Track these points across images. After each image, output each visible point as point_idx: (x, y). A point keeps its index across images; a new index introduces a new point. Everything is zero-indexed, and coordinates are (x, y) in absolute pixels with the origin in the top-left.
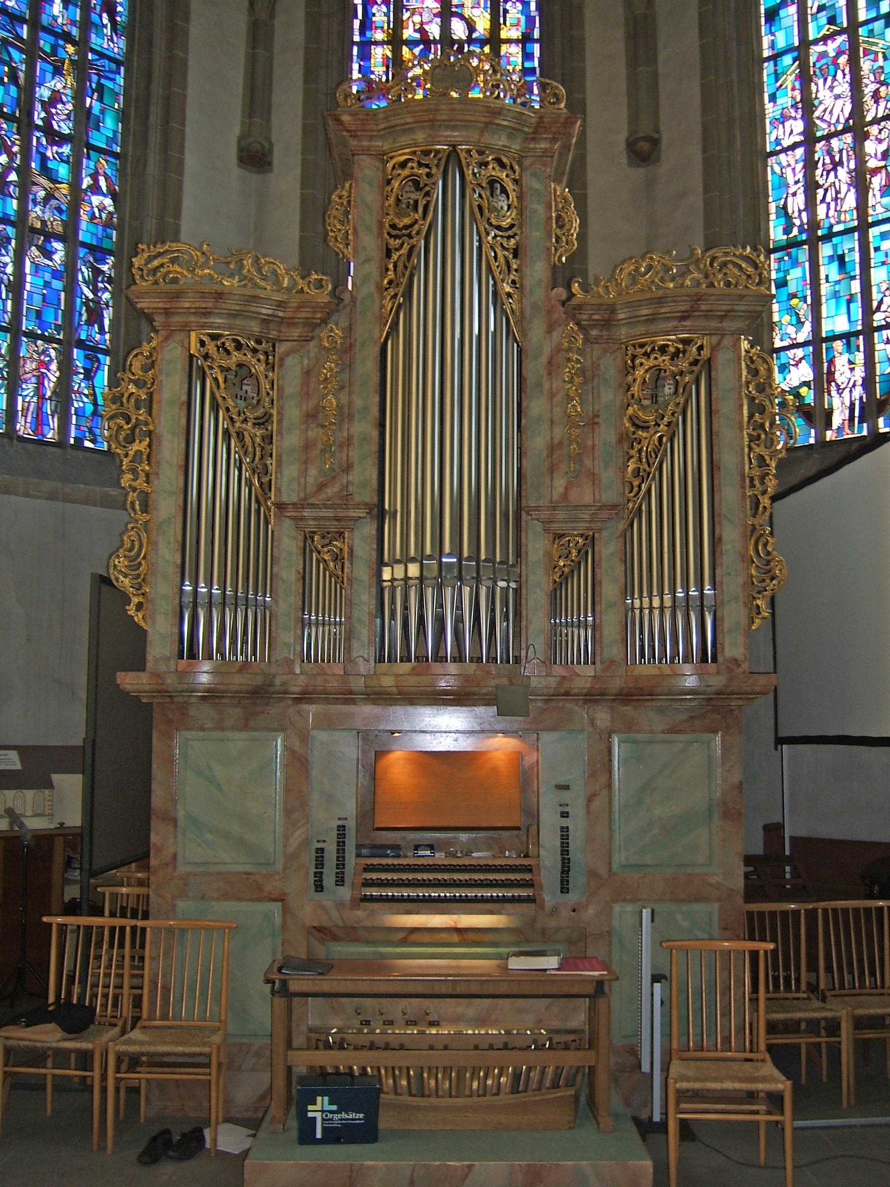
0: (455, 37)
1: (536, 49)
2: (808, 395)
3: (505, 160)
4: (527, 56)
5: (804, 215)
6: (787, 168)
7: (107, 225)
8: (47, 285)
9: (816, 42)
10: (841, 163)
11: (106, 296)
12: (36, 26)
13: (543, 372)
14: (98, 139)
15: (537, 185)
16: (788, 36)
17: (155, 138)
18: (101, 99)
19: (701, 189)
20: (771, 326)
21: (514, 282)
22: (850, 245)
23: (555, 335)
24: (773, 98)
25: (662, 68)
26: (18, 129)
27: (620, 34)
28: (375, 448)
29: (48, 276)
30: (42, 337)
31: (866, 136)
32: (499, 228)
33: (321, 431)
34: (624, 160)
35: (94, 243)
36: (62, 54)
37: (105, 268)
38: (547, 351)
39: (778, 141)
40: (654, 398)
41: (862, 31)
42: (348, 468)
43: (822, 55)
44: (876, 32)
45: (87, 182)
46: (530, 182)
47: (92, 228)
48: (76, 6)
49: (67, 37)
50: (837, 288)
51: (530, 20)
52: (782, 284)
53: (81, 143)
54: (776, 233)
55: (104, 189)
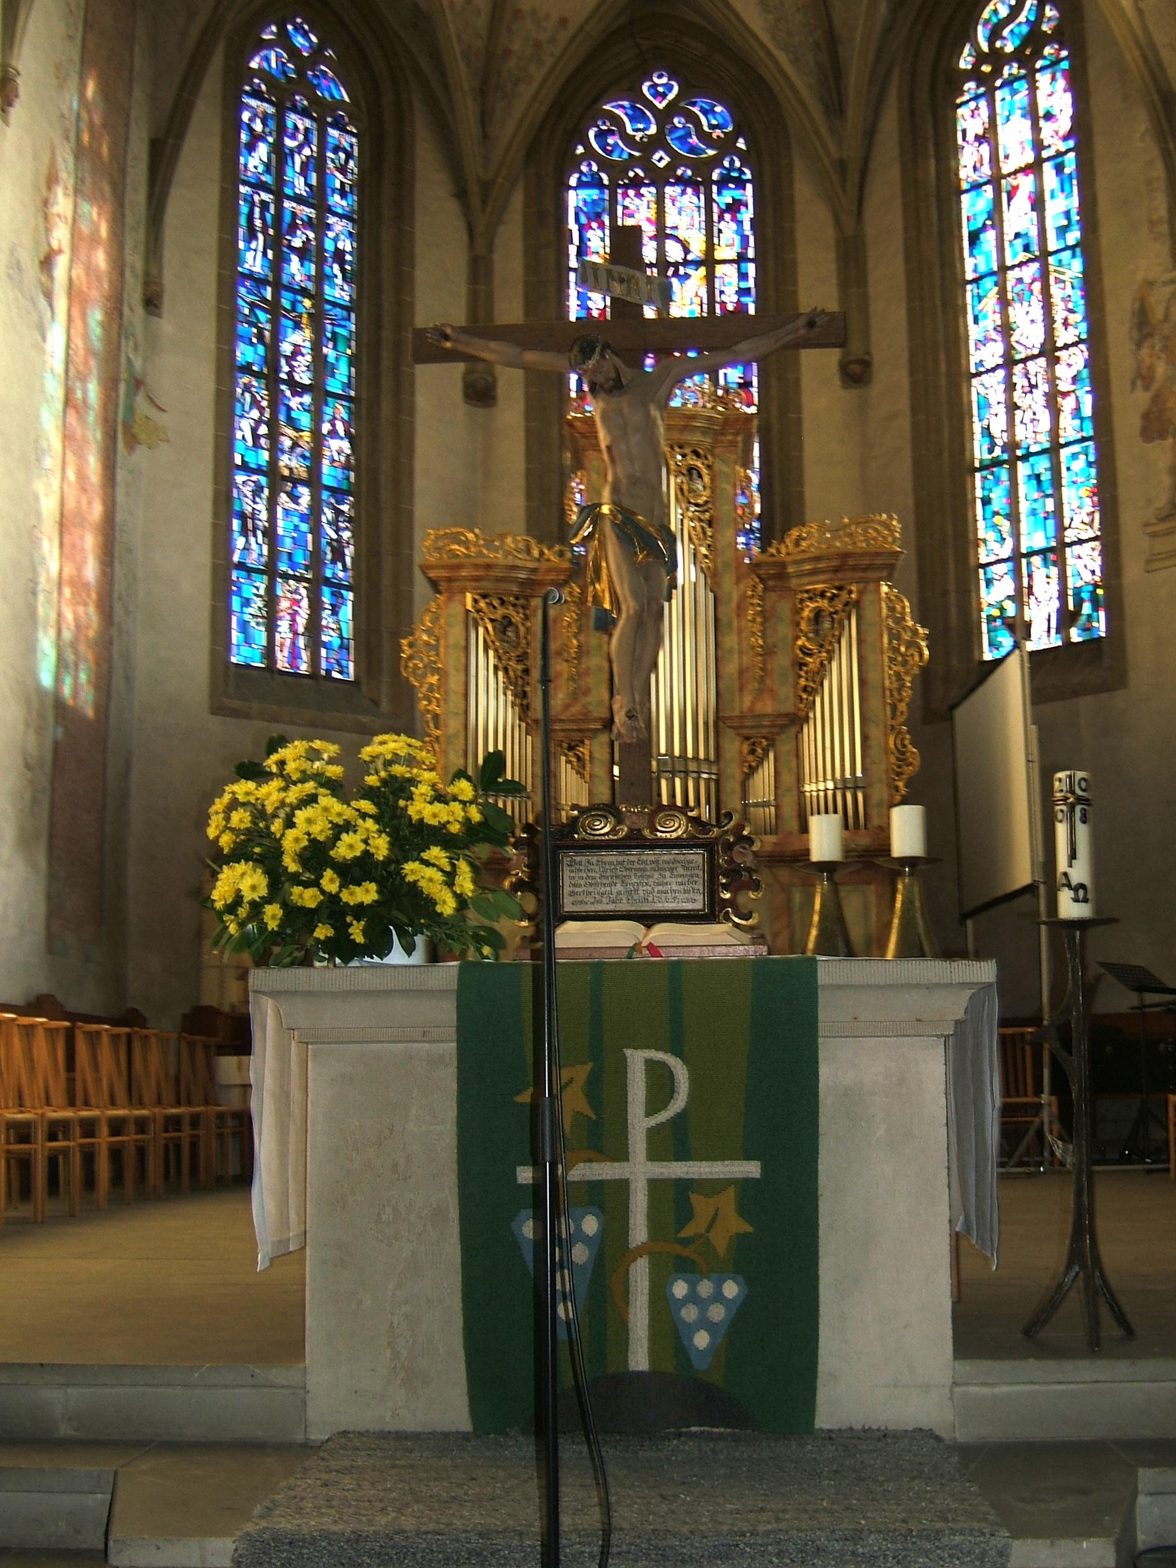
0: (669, 259)
1: (751, 269)
2: (1011, 609)
3: (701, 452)
4: (743, 276)
5: (1005, 435)
6: (988, 389)
7: (347, 467)
8: (296, 528)
9: (1013, 267)
10: (1036, 386)
11: (346, 535)
12: (278, 286)
13: (734, 614)
14: (334, 386)
15: (725, 469)
16: (988, 260)
17: (386, 383)
18: (335, 348)
19: (908, 412)
20: (977, 542)
21: (709, 546)
22: (1042, 464)
23: (742, 586)
24: (976, 321)
25: (872, 291)
26: (267, 385)
27: (832, 255)
28: (606, 676)
29: (296, 520)
30: (295, 578)
31: (1057, 360)
32: (697, 505)
33: (565, 664)
34: (837, 381)
35: (335, 485)
36: (300, 309)
37: (345, 508)
38: (735, 597)
39: (980, 363)
40: (817, 632)
41: (1051, 260)
42: (587, 692)
43: (1020, 281)
44: (1064, 262)
45: (326, 428)
46: (719, 466)
47: (333, 472)
48: (311, 261)
49: (304, 292)
50: (1035, 506)
51: (744, 239)
52: (986, 501)
53: (319, 392)
54: (980, 451)
55: (342, 433)
